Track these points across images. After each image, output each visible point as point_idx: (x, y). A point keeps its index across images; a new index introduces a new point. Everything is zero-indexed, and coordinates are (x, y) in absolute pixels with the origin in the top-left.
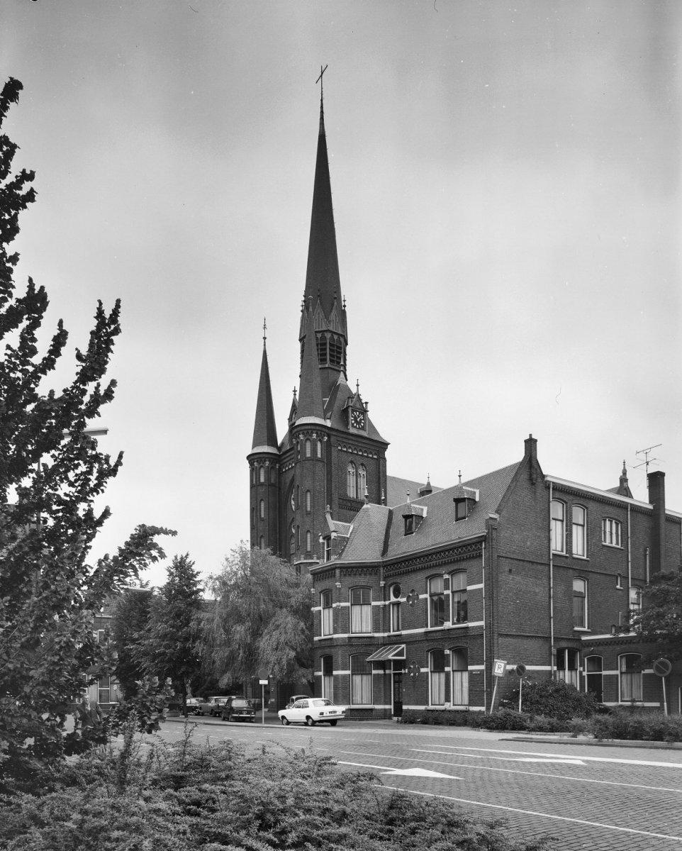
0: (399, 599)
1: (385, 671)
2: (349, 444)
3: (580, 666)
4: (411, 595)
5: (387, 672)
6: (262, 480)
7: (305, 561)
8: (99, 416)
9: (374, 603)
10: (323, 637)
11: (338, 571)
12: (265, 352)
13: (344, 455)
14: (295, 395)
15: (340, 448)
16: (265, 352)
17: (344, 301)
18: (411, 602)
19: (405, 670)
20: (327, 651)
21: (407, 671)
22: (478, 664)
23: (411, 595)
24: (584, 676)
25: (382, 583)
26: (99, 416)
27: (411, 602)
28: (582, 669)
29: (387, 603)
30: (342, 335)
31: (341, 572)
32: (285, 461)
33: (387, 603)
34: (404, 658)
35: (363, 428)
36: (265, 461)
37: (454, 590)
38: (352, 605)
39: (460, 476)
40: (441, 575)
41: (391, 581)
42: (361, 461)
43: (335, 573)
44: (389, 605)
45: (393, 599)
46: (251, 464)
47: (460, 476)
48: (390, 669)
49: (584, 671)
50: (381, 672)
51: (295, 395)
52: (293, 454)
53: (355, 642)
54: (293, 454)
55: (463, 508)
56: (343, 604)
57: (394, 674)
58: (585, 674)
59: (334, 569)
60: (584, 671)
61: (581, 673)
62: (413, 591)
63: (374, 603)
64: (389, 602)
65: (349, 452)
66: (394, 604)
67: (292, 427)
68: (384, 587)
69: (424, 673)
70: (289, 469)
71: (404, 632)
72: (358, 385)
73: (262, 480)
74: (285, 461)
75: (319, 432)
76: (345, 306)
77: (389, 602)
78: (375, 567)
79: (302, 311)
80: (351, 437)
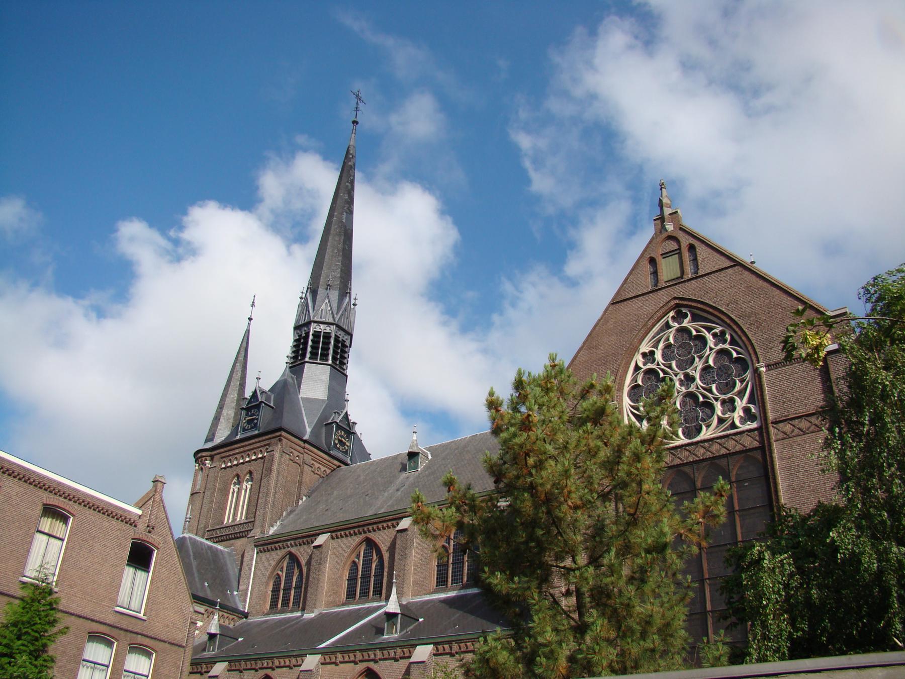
12: (247, 333)
16: (247, 333)
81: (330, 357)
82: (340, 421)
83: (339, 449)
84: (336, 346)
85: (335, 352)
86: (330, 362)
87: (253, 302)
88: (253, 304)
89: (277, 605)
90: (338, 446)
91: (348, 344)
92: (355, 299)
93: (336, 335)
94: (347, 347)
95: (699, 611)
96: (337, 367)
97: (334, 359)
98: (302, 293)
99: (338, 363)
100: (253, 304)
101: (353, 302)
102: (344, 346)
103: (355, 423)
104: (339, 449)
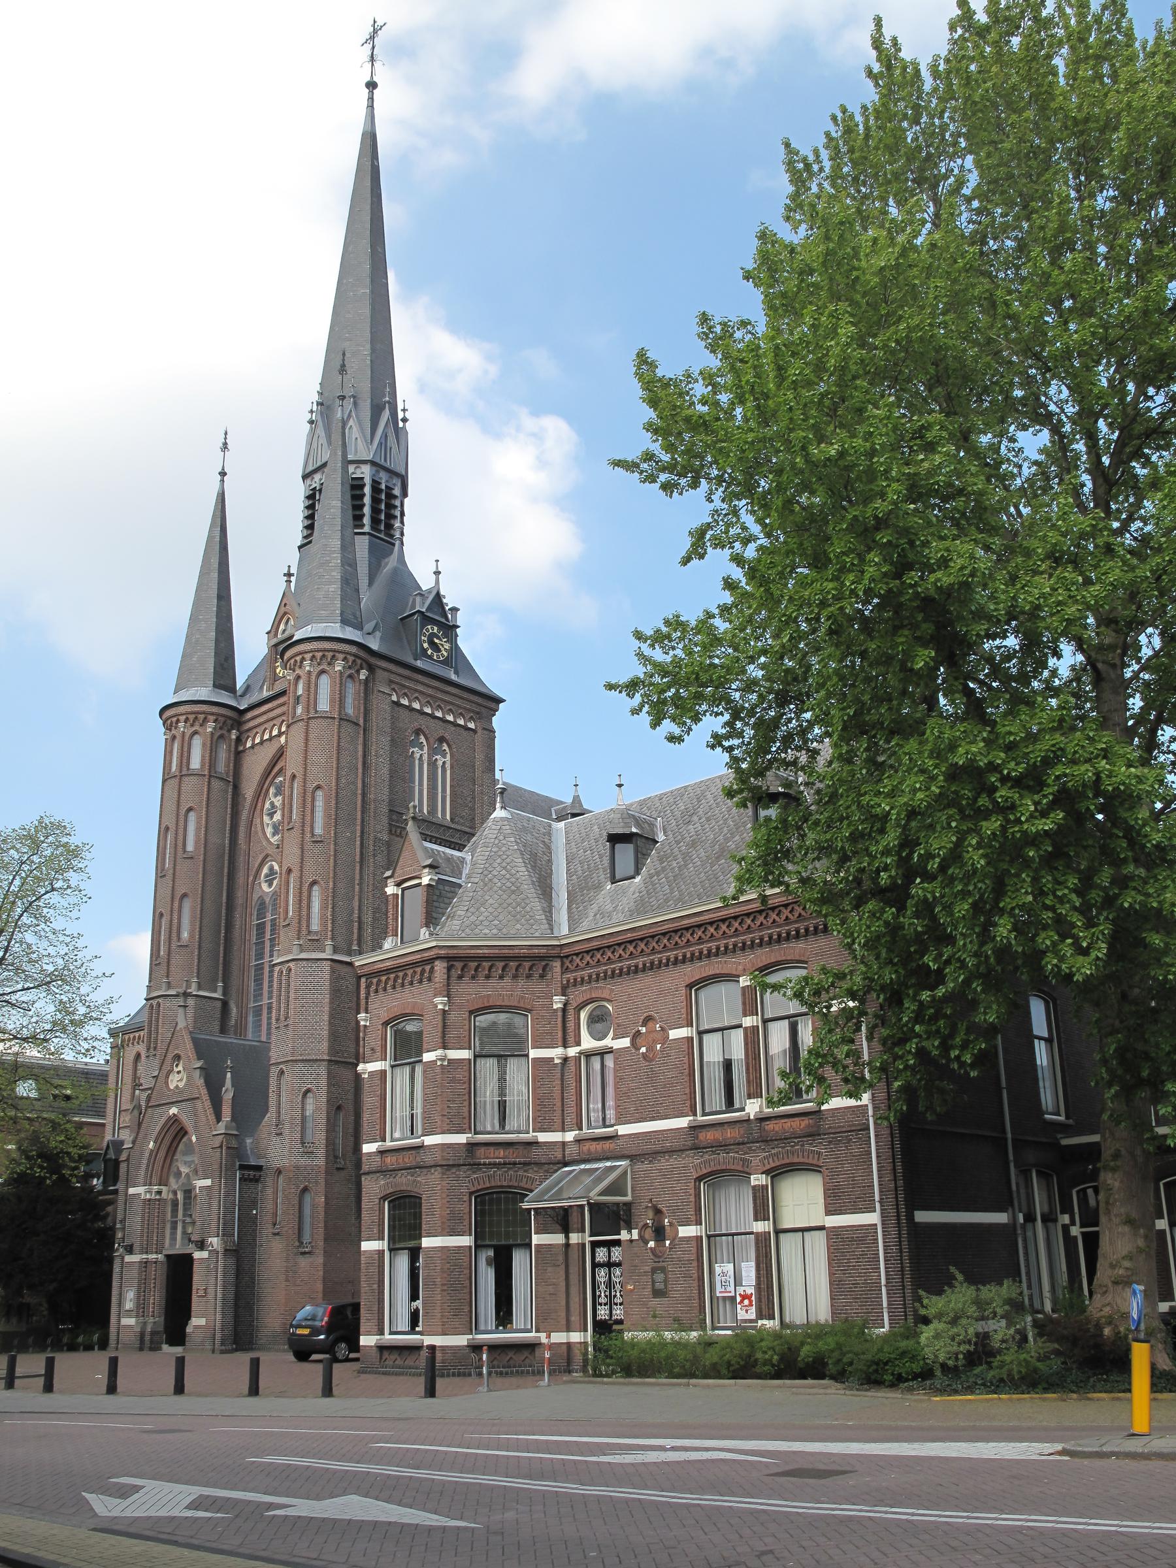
0: (608, 1042)
1: (567, 1237)
2: (416, 690)
3: (1063, 1212)
4: (644, 1030)
5: (575, 1238)
6: (195, 763)
7: (303, 956)
8: (704, 319)
9: (534, 1053)
10: (389, 1144)
11: (440, 966)
12: (221, 498)
13: (405, 714)
14: (289, 582)
15: (394, 698)
16: (221, 498)
17: (404, 410)
18: (643, 1050)
19: (630, 1232)
20: (403, 1182)
21: (635, 1234)
22: (855, 1210)
23: (644, 1030)
24: (1076, 1237)
25: (558, 1002)
26: (704, 319)
27: (643, 1050)
28: (1066, 1219)
29: (572, 1052)
30: (397, 475)
31: (449, 969)
32: (251, 724)
33: (572, 1052)
34: (629, 1198)
35: (446, 662)
36: (206, 720)
37: (701, 1029)
38: (475, 1056)
39: (576, 785)
40: (732, 978)
41: (579, 994)
42: (441, 733)
43: (432, 970)
44: (577, 1059)
45: (588, 1042)
46: (169, 725)
47: (576, 785)
48: (583, 1231)
49: (1073, 1223)
50: (558, 1239)
51: (289, 582)
52: (283, 704)
53: (482, 1156)
54: (283, 704)
55: (626, 853)
56: (454, 1054)
57: (595, 1245)
58: (1075, 1231)
59: (431, 961)
60: (1073, 1223)
61: (1066, 1229)
62: (647, 1020)
63: (534, 1053)
64: (578, 1049)
65: (414, 709)
66: (589, 1055)
67: (281, 648)
68: (564, 1010)
69: (688, 1239)
70: (262, 742)
71: (623, 1130)
72: (437, 573)
73: (195, 763)
74: (251, 724)
75: (351, 659)
76: (405, 420)
77: (578, 1049)
78: (541, 958)
79: (311, 422)
80: (420, 677)
81: (366, 520)
82: (429, 609)
83: (430, 657)
84: (375, 500)
85: (375, 511)
86: (367, 529)
87: (225, 444)
88: (225, 446)
89: (263, 953)
90: (429, 652)
91: (397, 492)
92: (404, 410)
93: (374, 481)
94: (395, 497)
95: (326, 1057)
96: (382, 536)
97: (375, 521)
98: (312, 412)
99: (382, 528)
100: (225, 446)
101: (401, 415)
102: (390, 496)
103: (455, 610)
104: (430, 657)
